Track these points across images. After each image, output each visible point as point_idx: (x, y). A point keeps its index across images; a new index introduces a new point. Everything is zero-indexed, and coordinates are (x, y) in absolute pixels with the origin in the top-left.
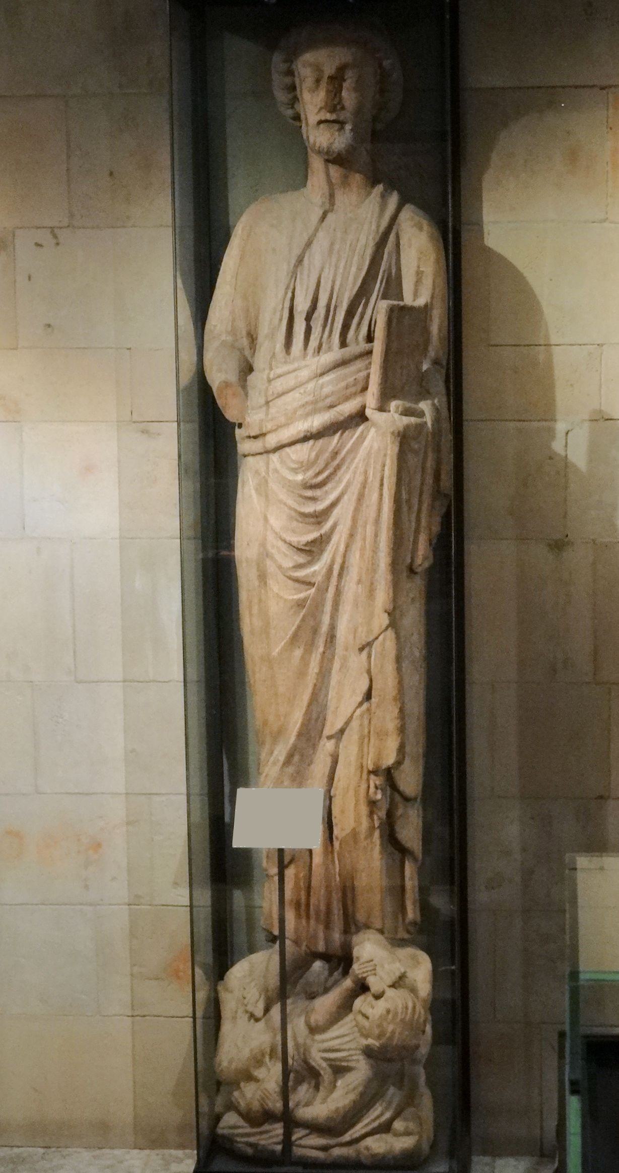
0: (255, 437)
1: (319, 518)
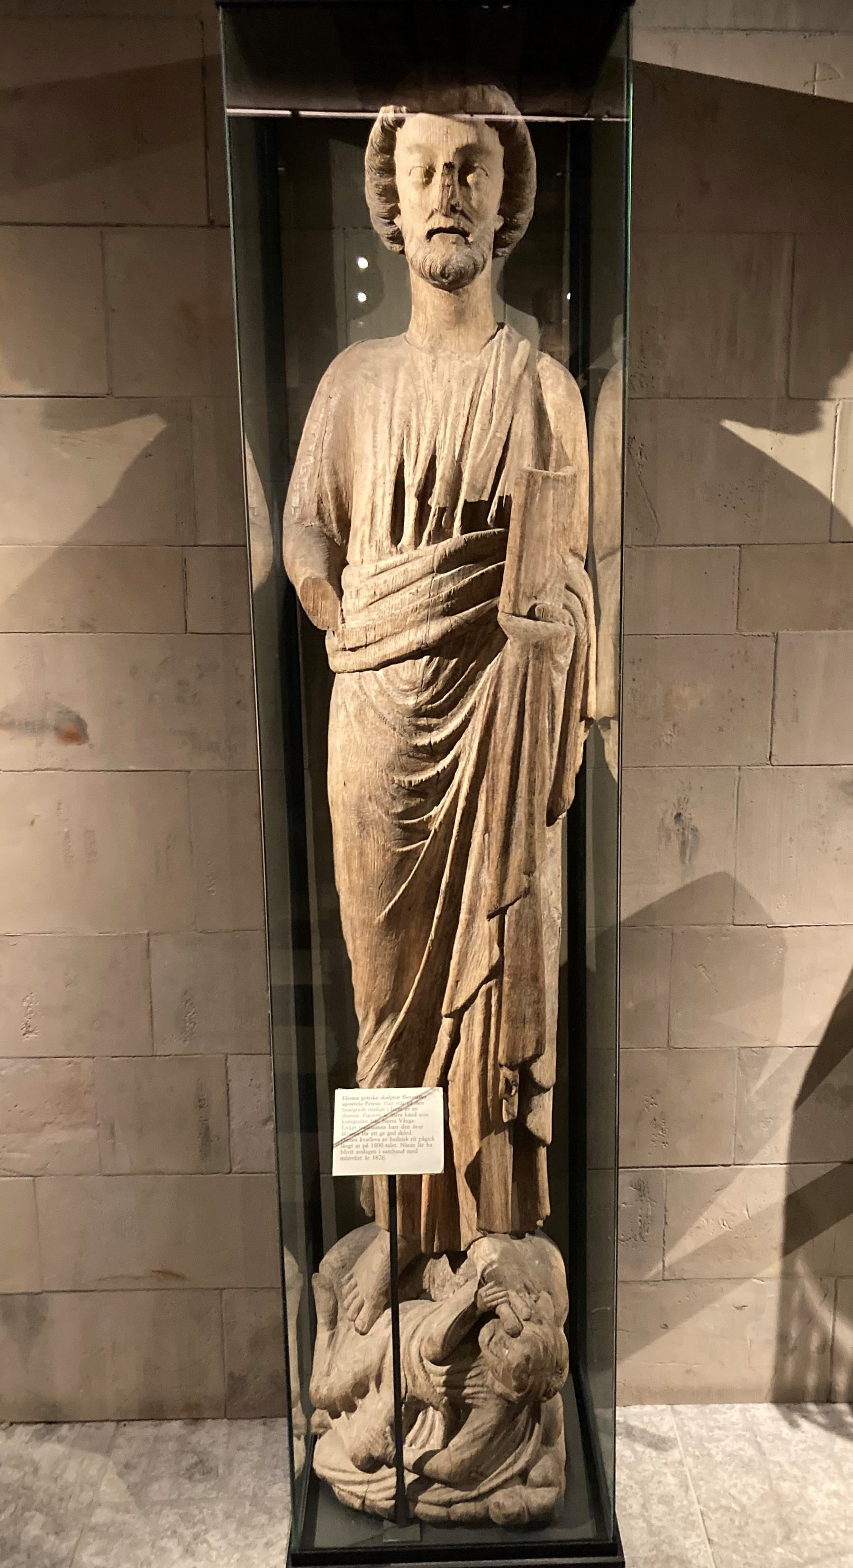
0: (353, 650)
1: (435, 752)
